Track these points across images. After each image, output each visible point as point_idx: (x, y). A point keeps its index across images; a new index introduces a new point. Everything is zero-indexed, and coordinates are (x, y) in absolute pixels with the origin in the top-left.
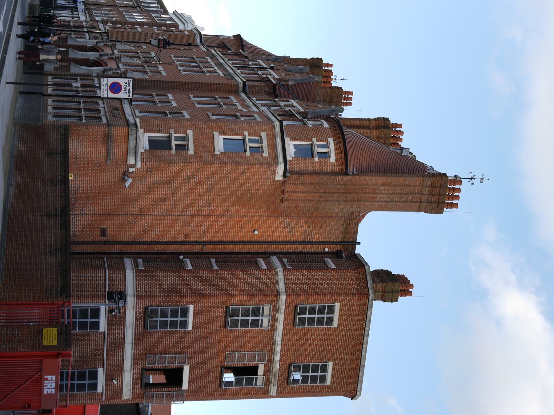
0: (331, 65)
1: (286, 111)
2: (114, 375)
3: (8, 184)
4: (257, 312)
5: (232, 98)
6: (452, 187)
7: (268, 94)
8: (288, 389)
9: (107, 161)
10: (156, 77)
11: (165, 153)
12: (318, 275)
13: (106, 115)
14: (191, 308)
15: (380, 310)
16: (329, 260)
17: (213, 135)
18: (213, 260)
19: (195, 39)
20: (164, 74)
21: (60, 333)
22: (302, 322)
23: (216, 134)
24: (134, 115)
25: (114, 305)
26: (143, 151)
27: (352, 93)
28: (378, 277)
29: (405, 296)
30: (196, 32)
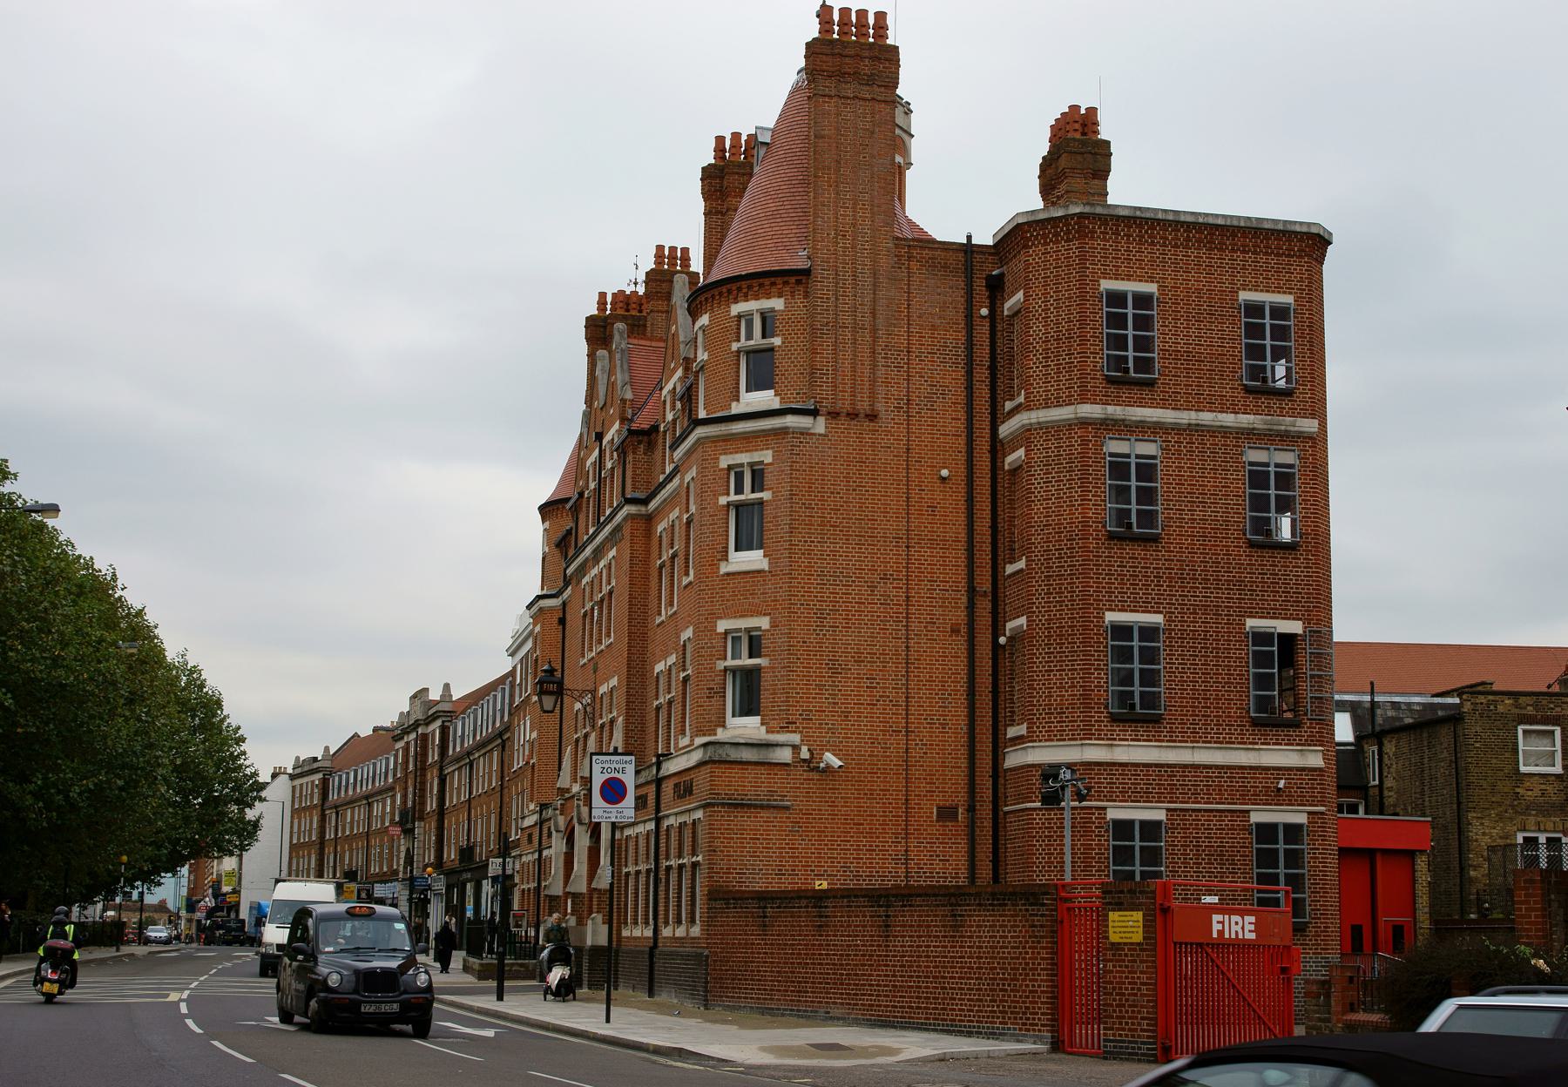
0: (603, 295)
1: (683, 409)
2: (1269, 787)
3: (826, 1019)
4: (1119, 468)
5: (660, 529)
6: (836, 28)
7: (651, 447)
8: (1309, 393)
9: (787, 808)
10: (620, 698)
11: (766, 681)
12: (1037, 329)
13: (689, 811)
14: (1111, 617)
15: (1126, 188)
16: (1007, 305)
17: (728, 574)
18: (1010, 569)
19: (551, 609)
20: (614, 682)
21: (1119, 906)
22: (1144, 365)
23: (724, 568)
24: (688, 750)
25: (1068, 792)
26: (763, 729)
27: (660, 248)
28: (1054, 188)
29: (1096, 124)
30: (535, 608)
